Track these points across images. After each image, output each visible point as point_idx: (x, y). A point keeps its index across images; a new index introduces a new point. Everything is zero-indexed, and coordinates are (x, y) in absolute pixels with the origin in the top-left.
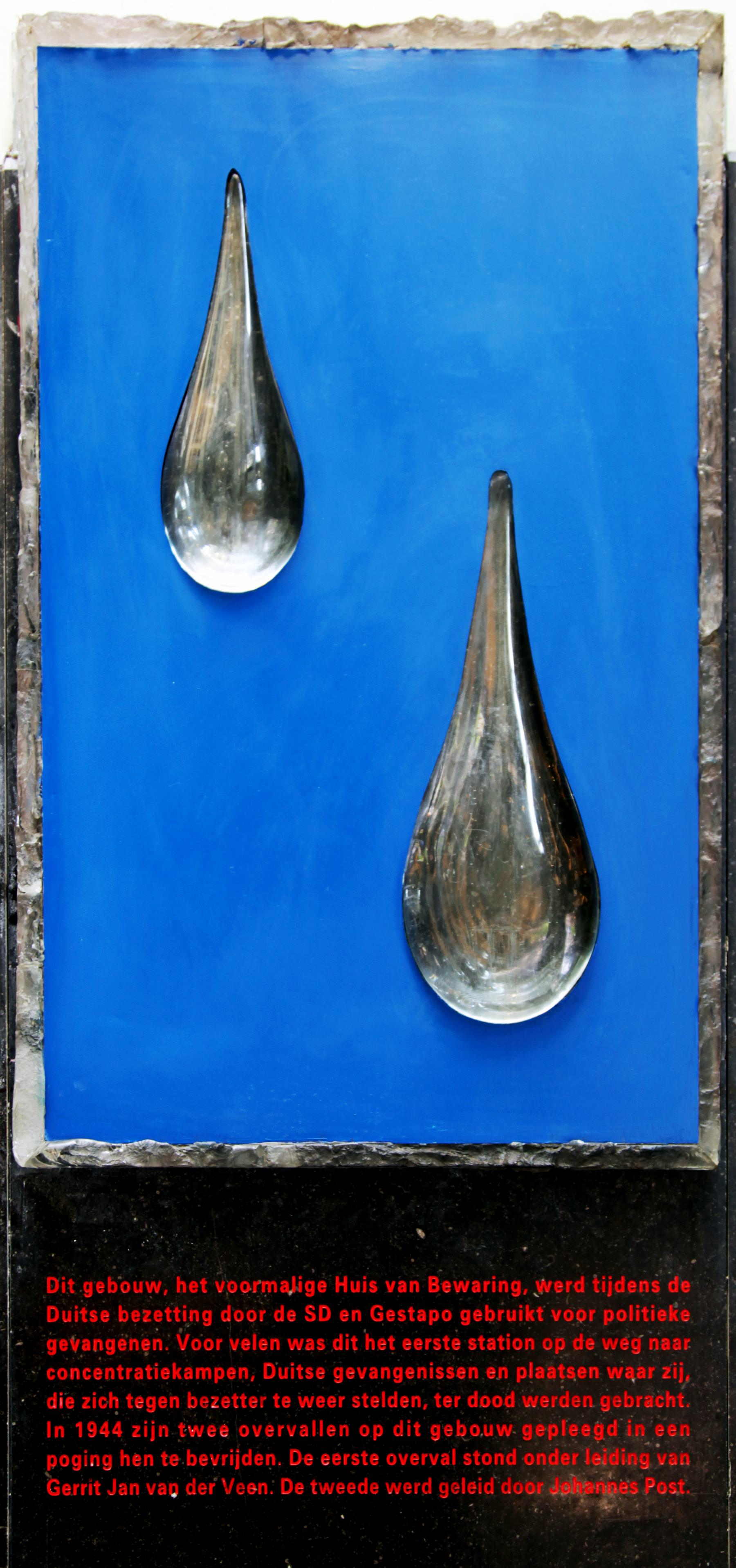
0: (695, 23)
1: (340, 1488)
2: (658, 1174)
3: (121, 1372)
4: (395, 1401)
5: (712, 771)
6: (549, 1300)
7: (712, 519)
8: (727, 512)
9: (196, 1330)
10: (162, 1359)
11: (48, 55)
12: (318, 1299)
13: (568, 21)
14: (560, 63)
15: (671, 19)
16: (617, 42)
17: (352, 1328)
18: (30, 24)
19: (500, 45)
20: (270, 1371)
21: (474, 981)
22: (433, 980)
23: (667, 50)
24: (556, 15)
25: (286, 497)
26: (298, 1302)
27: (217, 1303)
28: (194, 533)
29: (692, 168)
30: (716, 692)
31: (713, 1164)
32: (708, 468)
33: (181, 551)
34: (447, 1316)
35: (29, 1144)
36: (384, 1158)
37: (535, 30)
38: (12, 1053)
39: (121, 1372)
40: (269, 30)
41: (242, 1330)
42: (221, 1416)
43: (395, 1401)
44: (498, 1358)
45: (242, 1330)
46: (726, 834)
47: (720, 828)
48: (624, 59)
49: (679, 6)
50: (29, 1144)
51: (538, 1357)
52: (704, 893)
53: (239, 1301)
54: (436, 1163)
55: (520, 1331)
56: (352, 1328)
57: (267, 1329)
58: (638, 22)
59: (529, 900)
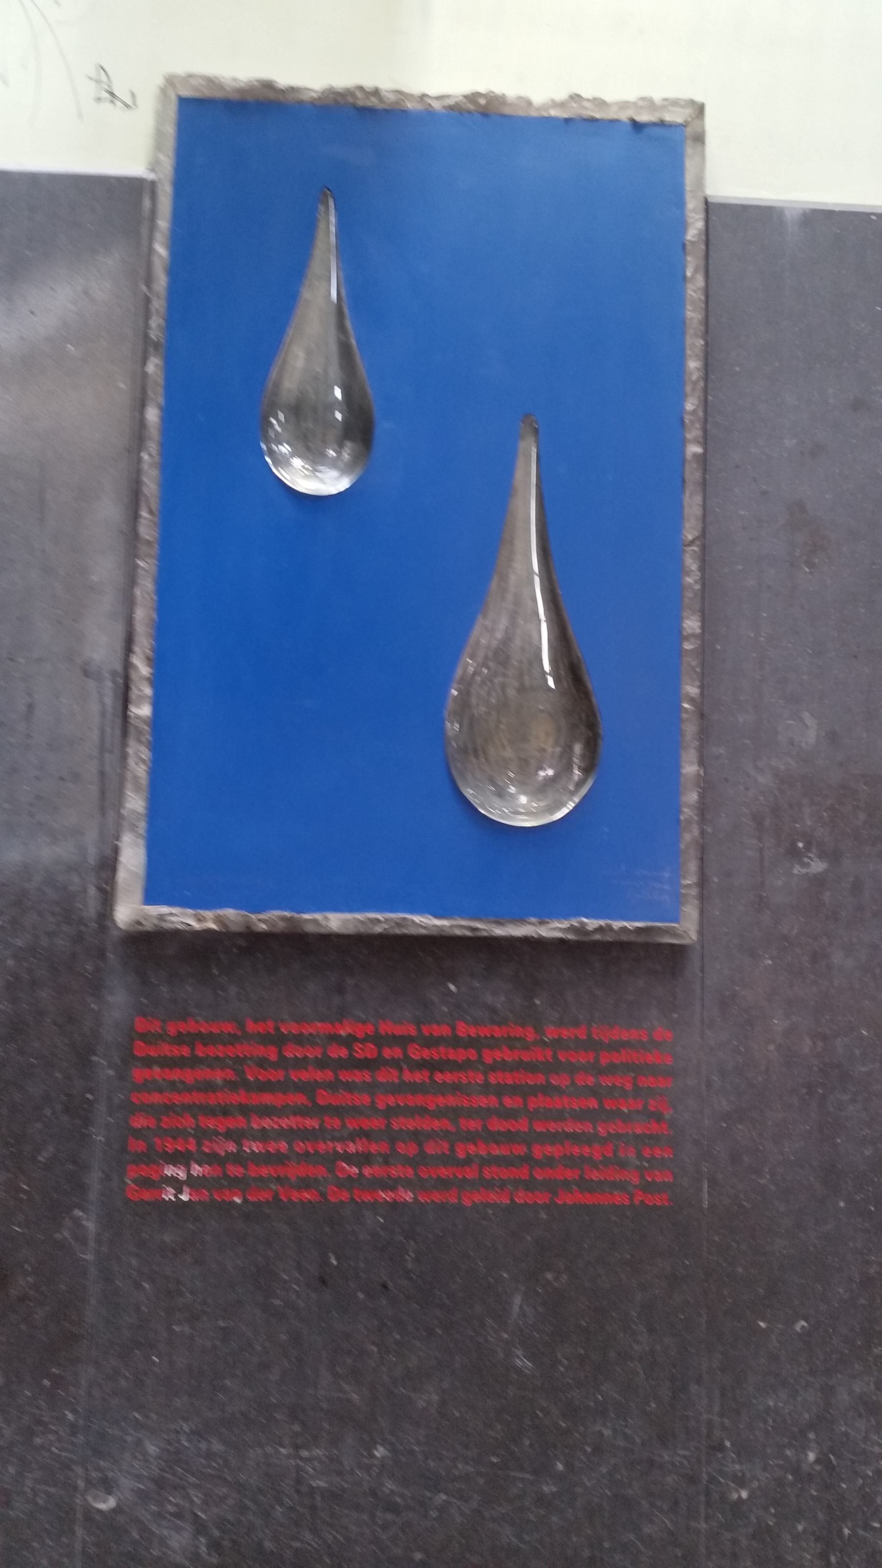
0: (683, 107)
1: (693, 365)
2: (646, 946)
3: (198, 1098)
4: (426, 1125)
5: (693, 640)
6: (558, 1043)
7: (695, 455)
8: (705, 450)
9: (262, 1063)
10: (232, 1086)
11: (184, 103)
12: (366, 1039)
13: (588, 100)
14: (579, 127)
15: (666, 103)
16: (624, 116)
17: (395, 1064)
18: (171, 81)
19: (534, 114)
20: (324, 1098)
21: (501, 793)
22: (469, 793)
23: (662, 124)
24: (579, 96)
25: (360, 429)
26: (349, 1041)
27: (279, 1040)
28: (285, 449)
29: (680, 204)
30: (696, 582)
31: (691, 938)
32: (692, 418)
33: (276, 463)
34: (472, 1054)
35: (127, 911)
36: (424, 928)
37: (562, 105)
38: (118, 838)
39: (198, 1098)
40: (359, 94)
41: (301, 1063)
42: (283, 1134)
43: (426, 1125)
44: (515, 1090)
45: (301, 1063)
46: (702, 687)
47: (698, 684)
48: (629, 128)
49: (672, 94)
50: (127, 911)
51: (546, 1089)
52: (142, 404)
53: (299, 1040)
54: (468, 933)
55: (532, 1068)
56: (395, 1064)
57: (322, 1064)
58: (641, 103)
59: (544, 735)
